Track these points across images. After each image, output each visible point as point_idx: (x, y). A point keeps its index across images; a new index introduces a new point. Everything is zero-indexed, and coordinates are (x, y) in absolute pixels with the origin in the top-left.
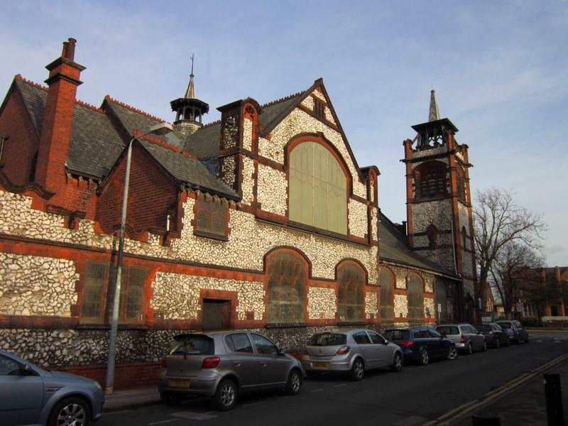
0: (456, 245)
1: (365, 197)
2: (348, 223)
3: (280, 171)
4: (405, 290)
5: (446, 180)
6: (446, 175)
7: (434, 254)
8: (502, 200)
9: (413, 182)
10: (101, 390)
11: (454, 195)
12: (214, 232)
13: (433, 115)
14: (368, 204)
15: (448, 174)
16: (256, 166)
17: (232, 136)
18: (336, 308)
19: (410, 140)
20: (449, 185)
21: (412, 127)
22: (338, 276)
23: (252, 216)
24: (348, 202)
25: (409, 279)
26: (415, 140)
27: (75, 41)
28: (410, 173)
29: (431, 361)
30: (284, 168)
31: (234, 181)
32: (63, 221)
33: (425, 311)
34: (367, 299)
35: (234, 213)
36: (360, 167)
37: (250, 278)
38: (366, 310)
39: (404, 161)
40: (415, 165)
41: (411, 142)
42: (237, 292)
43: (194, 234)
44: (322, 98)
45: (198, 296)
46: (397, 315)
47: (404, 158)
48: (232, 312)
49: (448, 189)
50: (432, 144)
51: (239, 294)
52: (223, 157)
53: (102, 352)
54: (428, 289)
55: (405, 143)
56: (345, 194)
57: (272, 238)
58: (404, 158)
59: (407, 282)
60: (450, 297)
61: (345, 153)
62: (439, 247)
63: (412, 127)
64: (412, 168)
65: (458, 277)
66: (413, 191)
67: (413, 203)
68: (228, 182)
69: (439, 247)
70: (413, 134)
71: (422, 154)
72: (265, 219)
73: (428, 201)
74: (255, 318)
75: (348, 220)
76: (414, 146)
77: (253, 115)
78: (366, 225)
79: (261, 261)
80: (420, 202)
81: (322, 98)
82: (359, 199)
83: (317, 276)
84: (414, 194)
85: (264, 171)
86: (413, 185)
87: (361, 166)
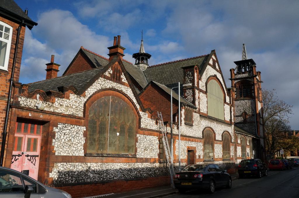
0: (257, 122)
1: (229, 102)
2: (224, 115)
3: (205, 94)
4: (240, 144)
5: (251, 90)
6: (252, 87)
7: (246, 126)
8: (268, 96)
9: (235, 90)
10: (200, 180)
11: (256, 97)
12: (189, 123)
13: (244, 56)
14: (230, 105)
15: (253, 87)
16: (199, 93)
17: (190, 80)
18: (222, 153)
19: (234, 69)
20: (253, 92)
21: (235, 62)
22: (223, 139)
23: (199, 115)
24: (224, 105)
25: (242, 139)
26: (236, 69)
27: (120, 36)
28: (234, 85)
29: (216, 189)
30: (206, 93)
31: (192, 100)
32: (155, 122)
33: (247, 154)
34: (231, 149)
35: (194, 114)
36: (227, 88)
37: (199, 141)
38: (231, 154)
39: (230, 79)
40: (236, 81)
41: (234, 70)
42: (196, 147)
43: (185, 124)
44: (215, 59)
45: (187, 149)
46: (238, 156)
47: (230, 78)
48: (195, 155)
49: (253, 94)
50: (243, 70)
51: (197, 148)
52: (186, 89)
53: (165, 171)
54: (248, 144)
55: (231, 70)
56: (223, 101)
57: (205, 123)
58: (230, 78)
59: (241, 140)
60: (255, 147)
61: (223, 83)
62: (249, 123)
63: (235, 62)
64: (235, 83)
65: (258, 137)
66: (235, 94)
67: (235, 101)
68: (189, 100)
69: (249, 123)
70: (235, 66)
71: (240, 76)
72: (204, 116)
73: (243, 100)
74: (201, 158)
75: (224, 113)
76: (235, 72)
77: (197, 71)
78: (230, 115)
79: (202, 134)
80: (238, 100)
81: (215, 59)
82: (228, 104)
83: (217, 139)
84: (236, 96)
85: (201, 94)
86: (235, 92)
87: (228, 87)
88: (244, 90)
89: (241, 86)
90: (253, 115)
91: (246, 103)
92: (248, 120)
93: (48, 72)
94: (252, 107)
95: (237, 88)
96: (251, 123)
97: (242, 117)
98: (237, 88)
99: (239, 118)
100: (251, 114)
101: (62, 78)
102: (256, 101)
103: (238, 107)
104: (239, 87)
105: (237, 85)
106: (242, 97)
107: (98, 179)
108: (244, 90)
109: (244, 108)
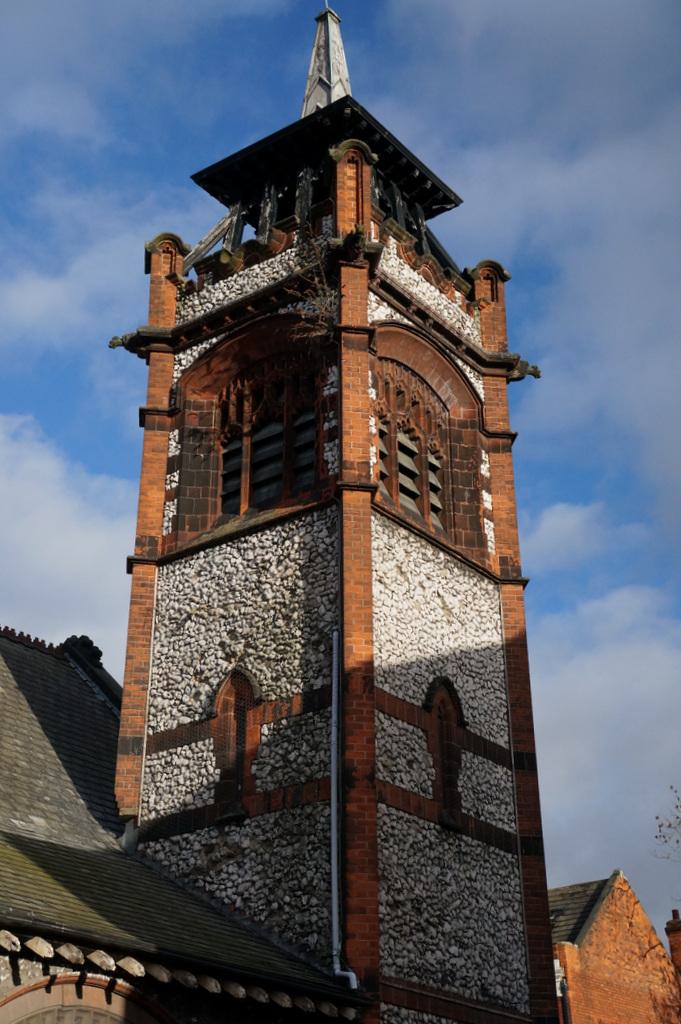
7: (236, 853)
62: (268, 802)
66: (169, 497)
69: (268, 802)
88: (265, 433)
89: (241, 397)
90: (314, 700)
91: (260, 569)
92: (263, 777)
93: (251, 509)
94: (308, 608)
95: (192, 423)
96: (301, 793)
97: (205, 747)
98: (192, 423)
99: (182, 755)
100: (297, 689)
101: (426, 501)
102: (349, 525)
103: (180, 626)
104: (216, 412)
105: (192, 398)
106: (237, 512)
107: (380, 818)
108: (265, 433)
109: (232, 633)
